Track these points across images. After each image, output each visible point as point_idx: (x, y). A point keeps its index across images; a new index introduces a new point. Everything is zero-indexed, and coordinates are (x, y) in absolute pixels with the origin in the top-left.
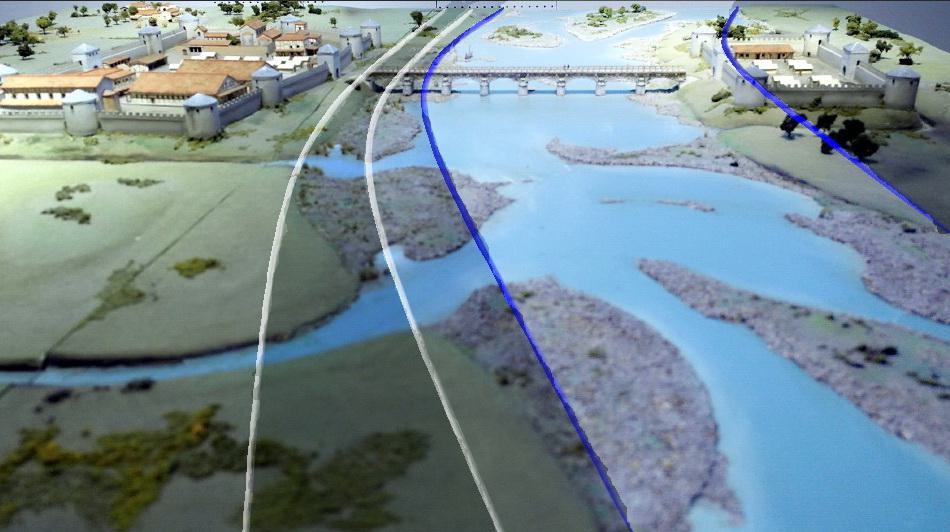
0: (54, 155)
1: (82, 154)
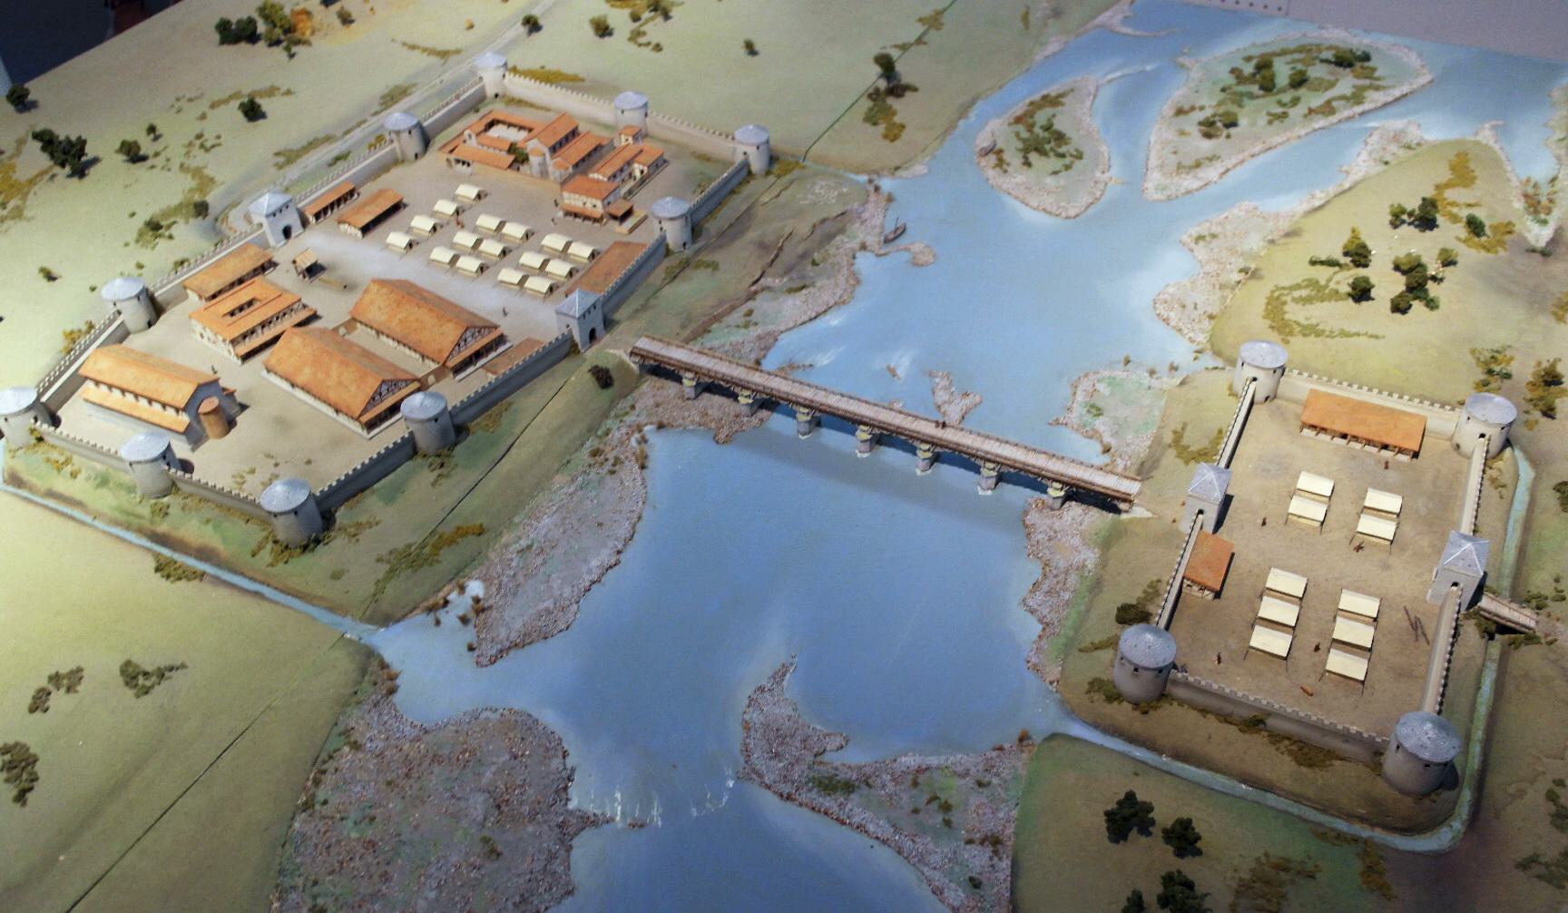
0: (117, 515)
1: (146, 524)
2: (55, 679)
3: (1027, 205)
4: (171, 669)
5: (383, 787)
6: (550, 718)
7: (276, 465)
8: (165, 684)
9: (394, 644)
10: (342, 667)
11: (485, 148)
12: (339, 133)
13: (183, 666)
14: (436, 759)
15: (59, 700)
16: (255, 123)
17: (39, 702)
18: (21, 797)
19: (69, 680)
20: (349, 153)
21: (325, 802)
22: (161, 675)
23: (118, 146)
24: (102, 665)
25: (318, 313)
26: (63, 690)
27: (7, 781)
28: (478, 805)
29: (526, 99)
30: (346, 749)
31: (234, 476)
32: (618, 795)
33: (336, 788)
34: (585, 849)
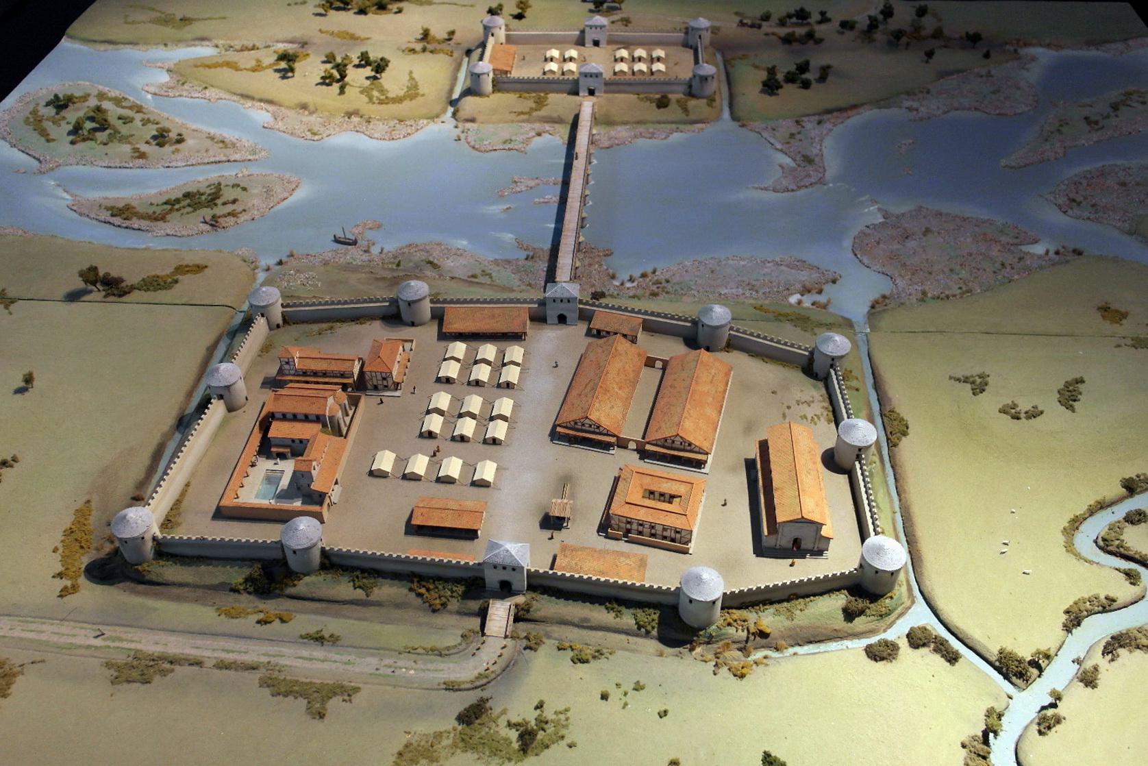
2: (1016, 417)
3: (237, 69)
4: (959, 380)
5: (934, 274)
6: (848, 243)
7: (789, 407)
8: (968, 374)
9: (857, 309)
10: (886, 322)
11: (177, 94)
12: (255, 676)
13: (951, 378)
14: (904, 265)
15: (1024, 406)
16: (120, 276)
17: (1034, 414)
18: (1082, 381)
19: (1011, 412)
20: (302, 637)
21: (960, 288)
22: (966, 380)
23: (425, 27)
24: (989, 403)
25: (770, 66)
26: (1018, 409)
27: (1080, 393)
28: (911, 244)
29: (176, 498)
30: (929, 295)
31: (816, 424)
32: (866, 210)
33: (950, 289)
34: (897, 210)
